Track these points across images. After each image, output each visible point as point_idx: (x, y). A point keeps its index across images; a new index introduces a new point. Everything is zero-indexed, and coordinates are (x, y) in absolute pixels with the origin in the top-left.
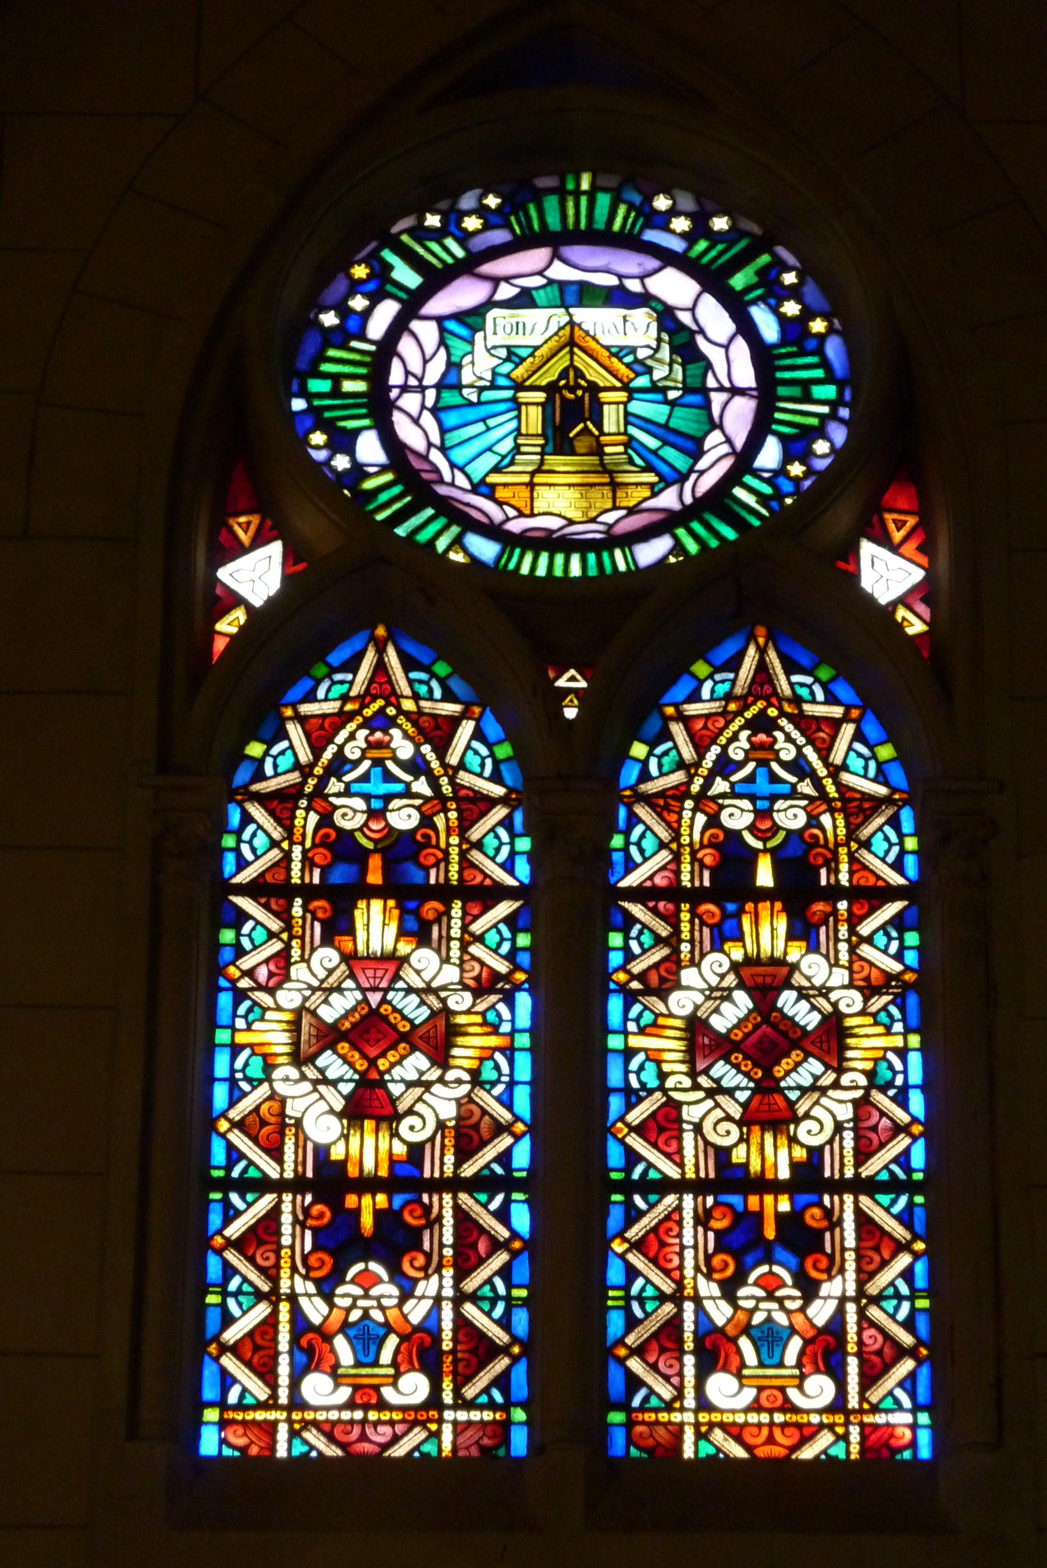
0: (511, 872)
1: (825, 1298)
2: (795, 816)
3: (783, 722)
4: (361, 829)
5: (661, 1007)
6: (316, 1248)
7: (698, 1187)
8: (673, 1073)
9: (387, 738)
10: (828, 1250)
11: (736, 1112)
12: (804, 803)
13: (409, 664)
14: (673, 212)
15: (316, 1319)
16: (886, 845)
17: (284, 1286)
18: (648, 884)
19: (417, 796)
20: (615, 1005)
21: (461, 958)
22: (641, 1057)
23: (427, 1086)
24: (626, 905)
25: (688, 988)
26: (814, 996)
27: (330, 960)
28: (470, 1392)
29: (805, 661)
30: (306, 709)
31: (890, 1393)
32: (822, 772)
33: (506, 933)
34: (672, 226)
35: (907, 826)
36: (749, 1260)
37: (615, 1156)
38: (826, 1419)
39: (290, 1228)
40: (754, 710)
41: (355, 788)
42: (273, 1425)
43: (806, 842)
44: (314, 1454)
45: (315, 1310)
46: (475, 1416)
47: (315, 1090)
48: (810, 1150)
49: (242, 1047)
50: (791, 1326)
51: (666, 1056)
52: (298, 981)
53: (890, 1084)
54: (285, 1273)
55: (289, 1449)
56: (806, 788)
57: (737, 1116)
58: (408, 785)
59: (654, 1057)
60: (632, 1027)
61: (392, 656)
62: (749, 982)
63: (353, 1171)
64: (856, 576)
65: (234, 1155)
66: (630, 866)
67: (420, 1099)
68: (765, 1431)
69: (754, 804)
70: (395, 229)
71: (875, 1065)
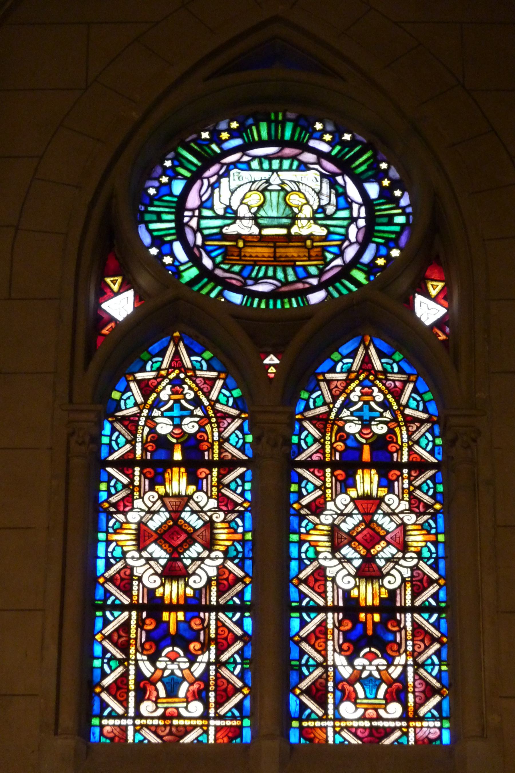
0: (243, 452)
1: (200, 663)
2: (382, 428)
3: (187, 380)
4: (170, 433)
5: (317, 521)
6: (147, 640)
8: (321, 552)
9: (370, 390)
12: (197, 419)
13: (381, 355)
14: (324, 131)
15: (148, 675)
16: (237, 439)
18: (310, 459)
19: (197, 416)
21: (409, 498)
22: (114, 544)
23: (202, 560)
24: (299, 470)
27: (345, 500)
28: (222, 711)
29: (196, 350)
30: (329, 376)
32: (206, 403)
34: (223, 139)
36: (163, 643)
37: (294, 595)
38: (398, 724)
42: (326, 727)
45: (147, 669)
47: (147, 563)
48: (195, 590)
49: (112, 541)
50: (381, 678)
51: (320, 544)
52: (331, 510)
53: (236, 557)
54: (132, 650)
58: (192, 411)
59: (314, 545)
60: (111, 530)
61: (372, 351)
63: (363, 604)
67: (199, 567)
68: (168, 729)
69: (173, 422)
70: (188, 139)
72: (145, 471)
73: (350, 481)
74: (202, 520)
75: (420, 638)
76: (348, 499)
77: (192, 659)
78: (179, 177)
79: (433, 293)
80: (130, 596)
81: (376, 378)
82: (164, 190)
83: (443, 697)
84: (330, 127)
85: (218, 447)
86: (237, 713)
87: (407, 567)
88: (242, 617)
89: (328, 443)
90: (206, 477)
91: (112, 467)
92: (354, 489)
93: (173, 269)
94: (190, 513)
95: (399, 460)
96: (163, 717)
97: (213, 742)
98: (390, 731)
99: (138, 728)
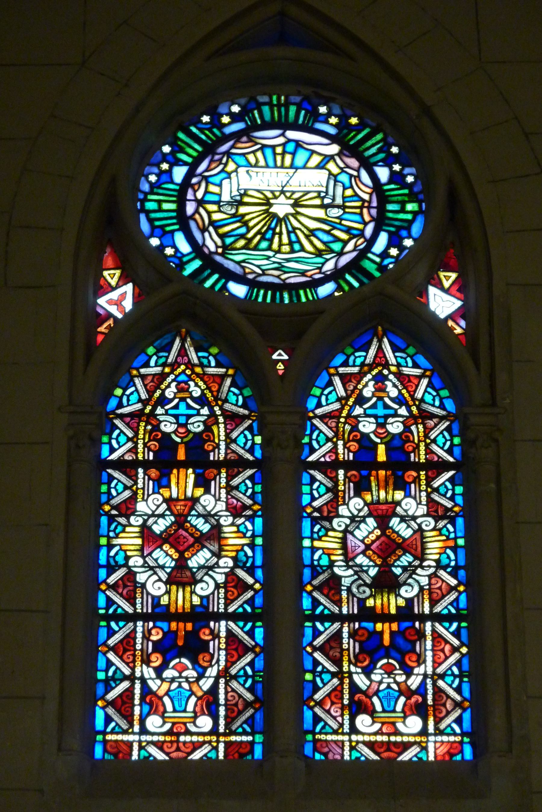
0: (252, 454)
2: (398, 426)
7: (350, 618)
9: (186, 386)
10: (211, 651)
11: (164, 577)
12: (401, 419)
13: (395, 349)
16: (444, 440)
17: (345, 668)
20: (306, 524)
21: (227, 498)
22: (117, 548)
25: (343, 517)
26: (408, 520)
30: (143, 371)
31: (449, 725)
33: (449, 486)
35: (455, 431)
36: (168, 656)
38: (418, 739)
39: (347, 640)
40: (374, 372)
41: (369, 412)
42: (343, 742)
43: (403, 439)
44: (363, 758)
45: (361, 681)
46: (445, 738)
48: (406, 600)
49: (318, 549)
53: (448, 566)
55: (350, 756)
56: (403, 411)
57: (164, 580)
58: (396, 410)
62: (375, 513)
63: (173, 610)
64: (427, 304)
65: (110, 602)
66: (313, 450)
68: (175, 745)
69: (377, 420)
71: (237, 554)
72: (349, 474)
73: (164, 482)
74: (210, 524)
75: (234, 647)
76: (161, 499)
77: (409, 672)
78: (181, 163)
79: (447, 284)
80: (134, 605)
81: (193, 372)
82: (164, 178)
83: (464, 710)
84: (337, 110)
85: (424, 448)
86: (248, 729)
87: (221, 573)
88: (253, 628)
89: (141, 442)
90: (215, 479)
91: (114, 469)
92: (168, 489)
93: (177, 261)
94: (196, 517)
95: (417, 460)
96: (170, 733)
97: (433, 759)
98: (406, 746)
99: (144, 744)
